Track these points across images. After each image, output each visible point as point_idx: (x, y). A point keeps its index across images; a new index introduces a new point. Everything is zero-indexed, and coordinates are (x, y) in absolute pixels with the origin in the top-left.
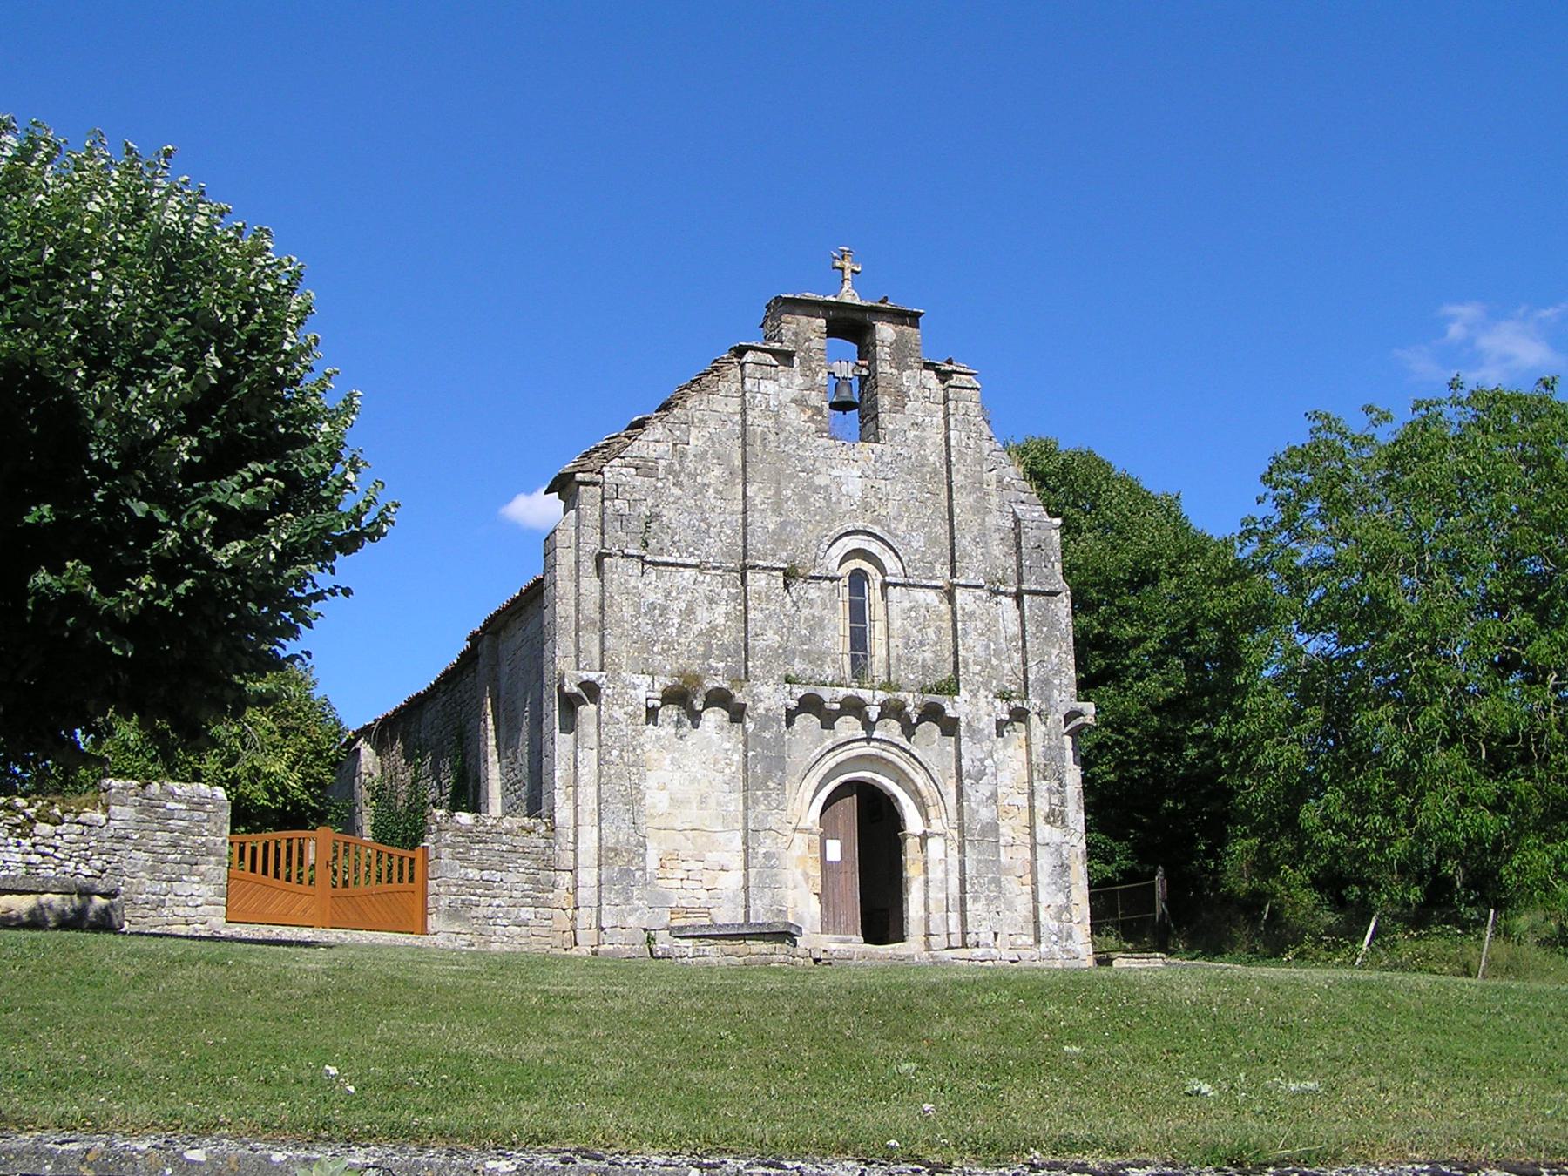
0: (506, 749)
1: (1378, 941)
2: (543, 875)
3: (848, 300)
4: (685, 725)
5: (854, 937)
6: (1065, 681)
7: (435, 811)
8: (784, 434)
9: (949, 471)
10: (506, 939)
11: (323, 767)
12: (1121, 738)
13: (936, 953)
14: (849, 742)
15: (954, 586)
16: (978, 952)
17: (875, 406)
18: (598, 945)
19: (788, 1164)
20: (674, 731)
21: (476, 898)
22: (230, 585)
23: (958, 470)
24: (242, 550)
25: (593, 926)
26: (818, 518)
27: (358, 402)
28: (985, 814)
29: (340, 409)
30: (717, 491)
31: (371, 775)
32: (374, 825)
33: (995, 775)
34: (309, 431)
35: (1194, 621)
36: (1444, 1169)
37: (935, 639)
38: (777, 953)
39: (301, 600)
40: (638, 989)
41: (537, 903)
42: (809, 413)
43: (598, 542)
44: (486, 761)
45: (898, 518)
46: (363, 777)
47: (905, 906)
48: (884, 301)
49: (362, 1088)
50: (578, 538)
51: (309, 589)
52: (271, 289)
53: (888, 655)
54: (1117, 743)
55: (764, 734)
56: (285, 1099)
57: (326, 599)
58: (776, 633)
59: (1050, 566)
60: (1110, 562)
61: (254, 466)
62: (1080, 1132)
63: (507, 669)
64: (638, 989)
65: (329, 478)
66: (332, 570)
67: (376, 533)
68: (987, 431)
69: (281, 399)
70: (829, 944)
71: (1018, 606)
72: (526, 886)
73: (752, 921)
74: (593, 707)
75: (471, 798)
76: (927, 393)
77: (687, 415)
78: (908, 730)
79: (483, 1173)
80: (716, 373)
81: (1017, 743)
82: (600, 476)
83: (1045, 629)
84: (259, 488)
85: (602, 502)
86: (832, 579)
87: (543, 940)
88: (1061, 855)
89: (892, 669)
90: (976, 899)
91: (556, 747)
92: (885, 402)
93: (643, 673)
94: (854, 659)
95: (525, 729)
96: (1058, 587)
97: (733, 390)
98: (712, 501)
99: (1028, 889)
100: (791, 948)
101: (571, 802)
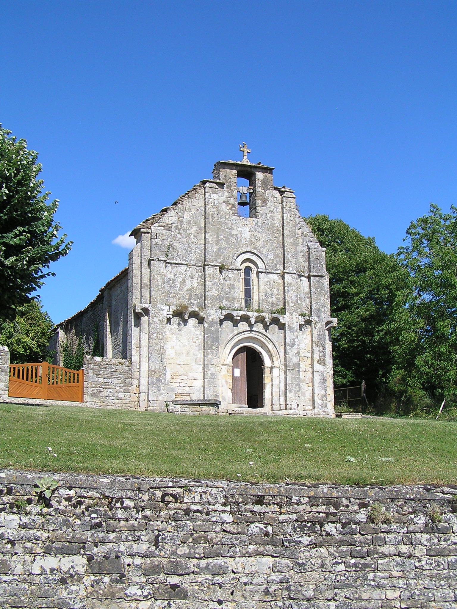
0: (114, 333)
1: (445, 410)
2: (127, 380)
3: (245, 163)
4: (181, 325)
5: (244, 406)
6: (326, 310)
7: (87, 356)
8: (220, 214)
9: (283, 229)
10: (113, 404)
11: (45, 339)
12: (350, 331)
13: (275, 412)
14: (243, 332)
15: (284, 273)
16: (291, 412)
17: (255, 204)
18: (148, 407)
19: (203, 482)
20: (177, 327)
21: (102, 389)
22: (10, 273)
23: (287, 229)
24: (15, 260)
25: (146, 400)
26: (233, 246)
27: (58, 204)
28: (295, 360)
29: (51, 206)
30: (194, 236)
31: (63, 342)
32: (64, 361)
33: (299, 345)
34: (40, 215)
35: (378, 286)
36: (428, 487)
37: (277, 293)
38: (212, 410)
39: (37, 278)
40: (156, 422)
41: (125, 391)
42: (230, 206)
43: (149, 255)
44: (106, 337)
45: (264, 247)
46: (60, 343)
47: (264, 394)
48: (259, 164)
49: (58, 455)
50: (141, 254)
51: (40, 274)
52: (26, 163)
53: (259, 299)
54: (349, 333)
55: (211, 329)
56: (32, 458)
57: (46, 277)
58: (216, 290)
59: (321, 266)
60: (347, 264)
61: (20, 229)
62: (304, 473)
63: (115, 303)
64: (156, 422)
65: (47, 233)
66: (48, 267)
67: (64, 254)
68: (298, 214)
69: (30, 204)
70: (235, 408)
71: (309, 281)
72: (121, 385)
73: (206, 399)
74: (146, 318)
75: (101, 351)
76: (275, 199)
77: (183, 207)
78: (266, 327)
79: (99, 483)
80: (194, 191)
81: (307, 333)
82: (150, 230)
83: (319, 290)
84: (21, 237)
85: (151, 240)
86: (238, 270)
87: (127, 405)
88: (323, 375)
89: (260, 304)
90: (290, 392)
91: (133, 332)
92: (259, 202)
93: (166, 305)
94: (246, 301)
95: (121, 325)
96: (324, 274)
97: (201, 197)
98: (193, 240)
99: (311, 388)
100: (217, 409)
101: (138, 353)
